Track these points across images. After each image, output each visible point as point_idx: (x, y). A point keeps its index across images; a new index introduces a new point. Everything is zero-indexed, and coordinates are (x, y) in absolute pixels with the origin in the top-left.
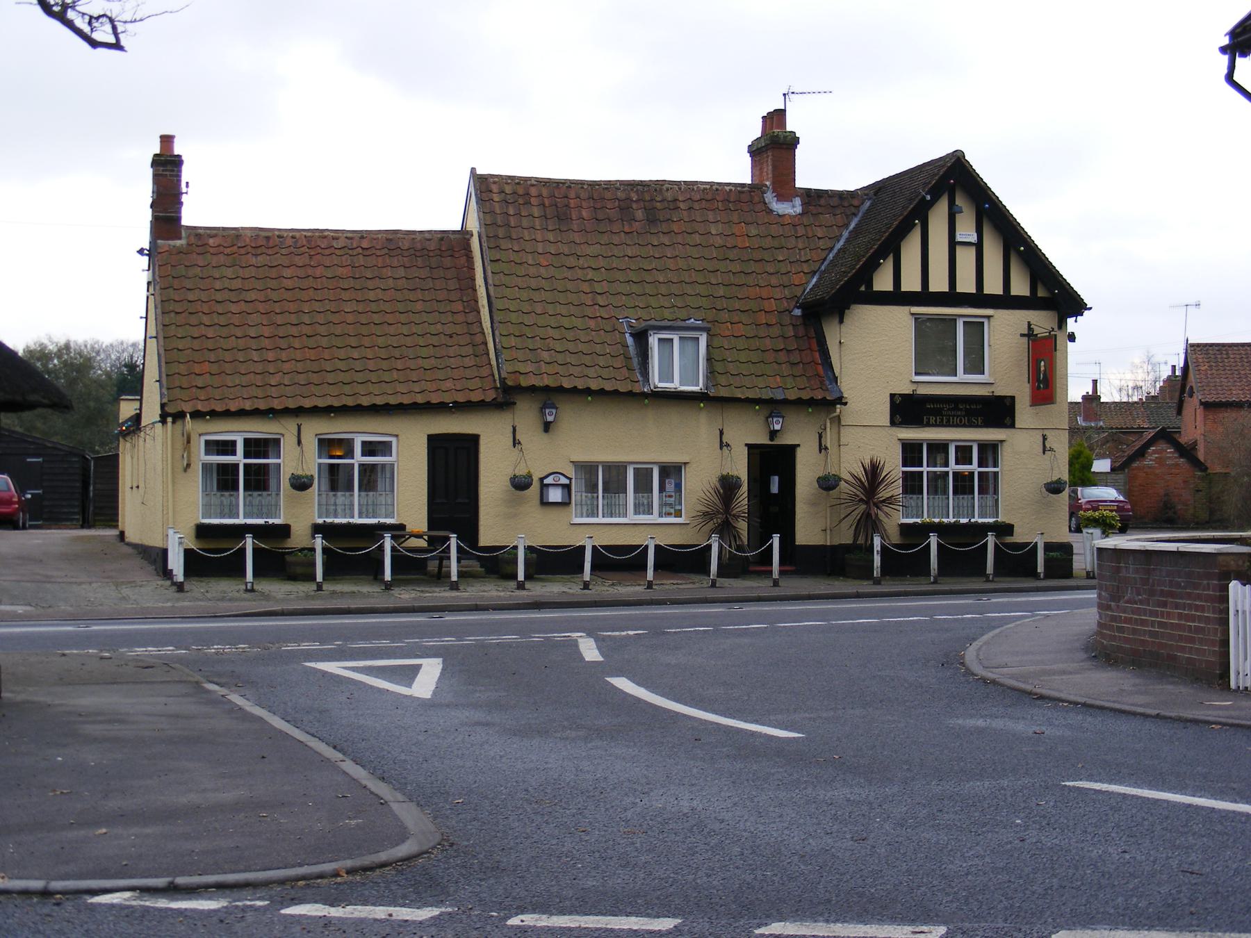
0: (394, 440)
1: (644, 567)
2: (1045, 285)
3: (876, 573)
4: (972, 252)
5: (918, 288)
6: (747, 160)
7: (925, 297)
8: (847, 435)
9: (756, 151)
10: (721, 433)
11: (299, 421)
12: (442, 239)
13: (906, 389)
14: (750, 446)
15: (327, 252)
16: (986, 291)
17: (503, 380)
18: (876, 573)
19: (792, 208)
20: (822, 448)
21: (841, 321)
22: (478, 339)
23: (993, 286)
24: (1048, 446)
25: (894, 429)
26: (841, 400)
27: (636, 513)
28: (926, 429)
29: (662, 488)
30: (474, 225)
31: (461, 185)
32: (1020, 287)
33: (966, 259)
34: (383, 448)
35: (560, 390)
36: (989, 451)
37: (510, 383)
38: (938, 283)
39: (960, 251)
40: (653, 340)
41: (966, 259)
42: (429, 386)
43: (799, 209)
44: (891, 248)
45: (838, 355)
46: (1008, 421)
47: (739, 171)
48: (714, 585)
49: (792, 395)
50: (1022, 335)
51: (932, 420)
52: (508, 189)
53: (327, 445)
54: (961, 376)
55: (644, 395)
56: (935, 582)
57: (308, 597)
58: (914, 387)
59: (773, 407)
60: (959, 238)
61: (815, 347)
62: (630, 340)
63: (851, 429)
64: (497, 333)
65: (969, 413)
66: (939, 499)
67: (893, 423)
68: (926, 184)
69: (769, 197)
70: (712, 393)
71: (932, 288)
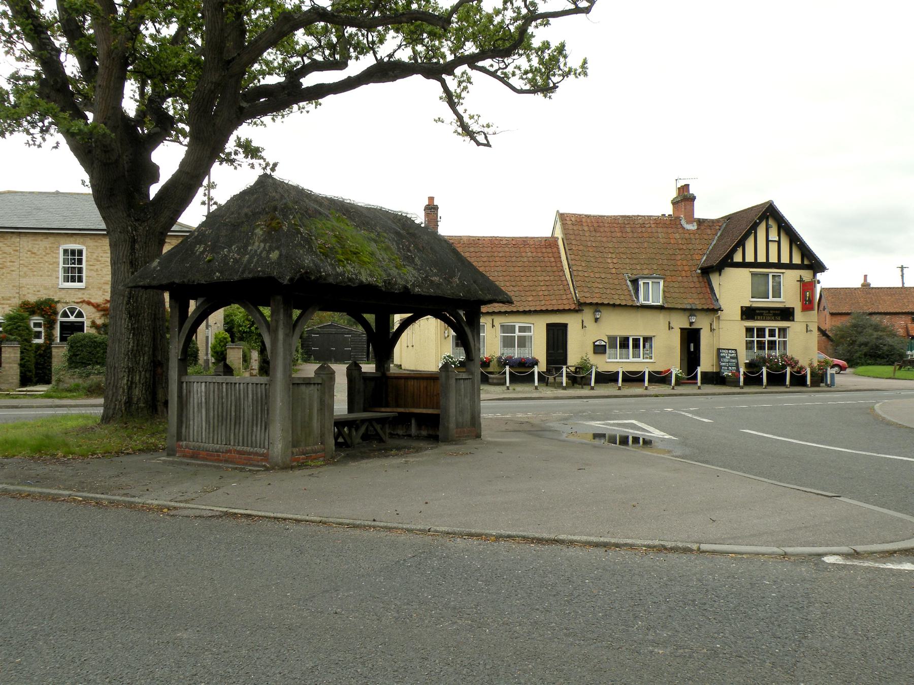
0: (532, 325)
1: (643, 381)
2: (808, 258)
3: (741, 384)
4: (776, 244)
5: (753, 261)
6: (671, 206)
7: (755, 265)
8: (722, 324)
9: (675, 203)
10: (669, 323)
11: (493, 317)
12: (546, 240)
13: (748, 305)
14: (682, 329)
15: (499, 246)
16: (747, 261)
17: (578, 301)
18: (741, 384)
19: (693, 227)
20: (712, 330)
21: (720, 275)
22: (565, 283)
23: (785, 260)
24: (809, 329)
25: (743, 322)
26: (720, 309)
27: (633, 357)
28: (756, 322)
29: (644, 347)
30: (559, 234)
31: (552, 218)
32: (797, 260)
33: (773, 247)
34: (528, 329)
35: (602, 304)
36: (783, 331)
37: (582, 301)
38: (762, 259)
39: (770, 244)
40: (641, 282)
41: (773, 247)
42: (547, 303)
43: (695, 227)
44: (741, 243)
45: (718, 290)
46: (791, 318)
47: (668, 210)
48: (673, 389)
49: (699, 307)
50: (798, 281)
51: (759, 318)
52: (573, 219)
53: (505, 328)
54: (771, 299)
55: (637, 307)
56: (765, 388)
57: (504, 393)
58: (751, 303)
59: (692, 311)
60: (770, 239)
61: (707, 286)
62: (629, 283)
63: (724, 322)
64: (574, 280)
65: (775, 315)
66: (613, 351)
67: (742, 319)
68: (756, 215)
69: (683, 222)
70: (666, 306)
71: (747, 260)
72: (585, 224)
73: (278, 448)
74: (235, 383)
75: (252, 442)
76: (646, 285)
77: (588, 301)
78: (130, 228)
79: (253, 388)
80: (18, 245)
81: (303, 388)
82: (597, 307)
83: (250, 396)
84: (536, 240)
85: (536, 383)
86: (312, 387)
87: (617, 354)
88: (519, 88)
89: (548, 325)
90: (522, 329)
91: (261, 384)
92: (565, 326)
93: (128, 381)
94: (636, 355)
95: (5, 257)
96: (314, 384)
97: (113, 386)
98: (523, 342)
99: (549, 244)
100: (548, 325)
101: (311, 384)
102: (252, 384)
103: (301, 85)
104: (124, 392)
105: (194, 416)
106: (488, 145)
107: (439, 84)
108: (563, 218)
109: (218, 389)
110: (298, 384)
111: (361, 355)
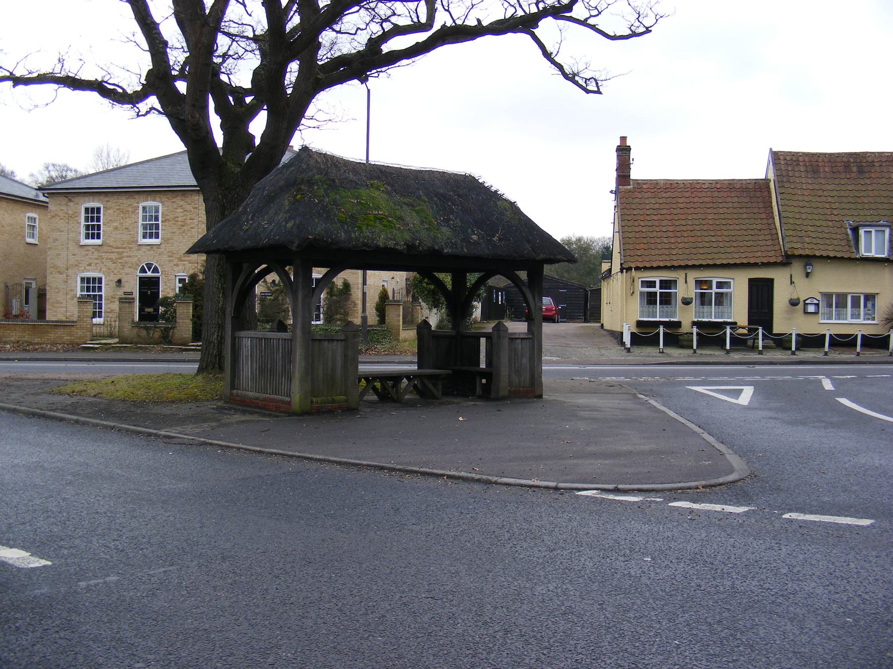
0: (731, 281)
1: (855, 345)
12: (756, 183)
17: (786, 252)
22: (773, 232)
29: (865, 306)
30: (771, 176)
35: (814, 257)
40: (862, 232)
42: (749, 255)
52: (788, 158)
57: (689, 356)
62: (849, 232)
64: (783, 228)
72: (801, 164)
73: (296, 395)
74: (271, 339)
75: (282, 393)
76: (880, 234)
77: (796, 253)
78: (220, 196)
79: (282, 342)
80: (197, 202)
81: (326, 343)
82: (808, 260)
83: (281, 350)
84: (744, 182)
85: (858, 349)
86: (335, 343)
87: (711, 312)
88: (612, 34)
89: (750, 280)
90: (720, 285)
91: (288, 340)
92: (771, 281)
93: (218, 336)
94: (856, 316)
95: (186, 215)
96: (338, 340)
97: (206, 341)
98: (721, 299)
99: (759, 187)
100: (750, 280)
101: (333, 340)
102: (282, 339)
103: (381, 50)
104: (214, 346)
105: (243, 368)
106: (598, 92)
107: (528, 37)
108: (777, 157)
109: (259, 343)
110: (320, 340)
111: (578, 312)
